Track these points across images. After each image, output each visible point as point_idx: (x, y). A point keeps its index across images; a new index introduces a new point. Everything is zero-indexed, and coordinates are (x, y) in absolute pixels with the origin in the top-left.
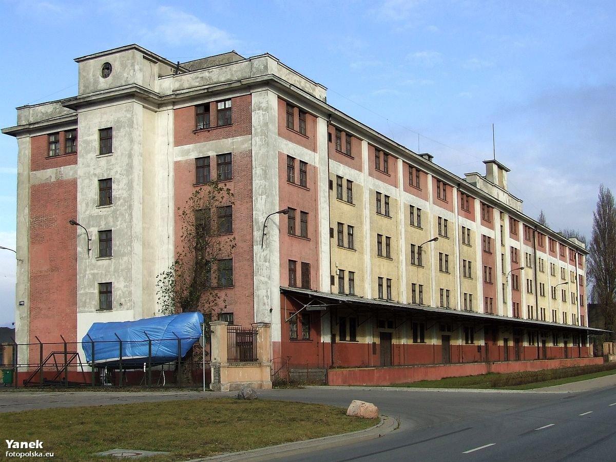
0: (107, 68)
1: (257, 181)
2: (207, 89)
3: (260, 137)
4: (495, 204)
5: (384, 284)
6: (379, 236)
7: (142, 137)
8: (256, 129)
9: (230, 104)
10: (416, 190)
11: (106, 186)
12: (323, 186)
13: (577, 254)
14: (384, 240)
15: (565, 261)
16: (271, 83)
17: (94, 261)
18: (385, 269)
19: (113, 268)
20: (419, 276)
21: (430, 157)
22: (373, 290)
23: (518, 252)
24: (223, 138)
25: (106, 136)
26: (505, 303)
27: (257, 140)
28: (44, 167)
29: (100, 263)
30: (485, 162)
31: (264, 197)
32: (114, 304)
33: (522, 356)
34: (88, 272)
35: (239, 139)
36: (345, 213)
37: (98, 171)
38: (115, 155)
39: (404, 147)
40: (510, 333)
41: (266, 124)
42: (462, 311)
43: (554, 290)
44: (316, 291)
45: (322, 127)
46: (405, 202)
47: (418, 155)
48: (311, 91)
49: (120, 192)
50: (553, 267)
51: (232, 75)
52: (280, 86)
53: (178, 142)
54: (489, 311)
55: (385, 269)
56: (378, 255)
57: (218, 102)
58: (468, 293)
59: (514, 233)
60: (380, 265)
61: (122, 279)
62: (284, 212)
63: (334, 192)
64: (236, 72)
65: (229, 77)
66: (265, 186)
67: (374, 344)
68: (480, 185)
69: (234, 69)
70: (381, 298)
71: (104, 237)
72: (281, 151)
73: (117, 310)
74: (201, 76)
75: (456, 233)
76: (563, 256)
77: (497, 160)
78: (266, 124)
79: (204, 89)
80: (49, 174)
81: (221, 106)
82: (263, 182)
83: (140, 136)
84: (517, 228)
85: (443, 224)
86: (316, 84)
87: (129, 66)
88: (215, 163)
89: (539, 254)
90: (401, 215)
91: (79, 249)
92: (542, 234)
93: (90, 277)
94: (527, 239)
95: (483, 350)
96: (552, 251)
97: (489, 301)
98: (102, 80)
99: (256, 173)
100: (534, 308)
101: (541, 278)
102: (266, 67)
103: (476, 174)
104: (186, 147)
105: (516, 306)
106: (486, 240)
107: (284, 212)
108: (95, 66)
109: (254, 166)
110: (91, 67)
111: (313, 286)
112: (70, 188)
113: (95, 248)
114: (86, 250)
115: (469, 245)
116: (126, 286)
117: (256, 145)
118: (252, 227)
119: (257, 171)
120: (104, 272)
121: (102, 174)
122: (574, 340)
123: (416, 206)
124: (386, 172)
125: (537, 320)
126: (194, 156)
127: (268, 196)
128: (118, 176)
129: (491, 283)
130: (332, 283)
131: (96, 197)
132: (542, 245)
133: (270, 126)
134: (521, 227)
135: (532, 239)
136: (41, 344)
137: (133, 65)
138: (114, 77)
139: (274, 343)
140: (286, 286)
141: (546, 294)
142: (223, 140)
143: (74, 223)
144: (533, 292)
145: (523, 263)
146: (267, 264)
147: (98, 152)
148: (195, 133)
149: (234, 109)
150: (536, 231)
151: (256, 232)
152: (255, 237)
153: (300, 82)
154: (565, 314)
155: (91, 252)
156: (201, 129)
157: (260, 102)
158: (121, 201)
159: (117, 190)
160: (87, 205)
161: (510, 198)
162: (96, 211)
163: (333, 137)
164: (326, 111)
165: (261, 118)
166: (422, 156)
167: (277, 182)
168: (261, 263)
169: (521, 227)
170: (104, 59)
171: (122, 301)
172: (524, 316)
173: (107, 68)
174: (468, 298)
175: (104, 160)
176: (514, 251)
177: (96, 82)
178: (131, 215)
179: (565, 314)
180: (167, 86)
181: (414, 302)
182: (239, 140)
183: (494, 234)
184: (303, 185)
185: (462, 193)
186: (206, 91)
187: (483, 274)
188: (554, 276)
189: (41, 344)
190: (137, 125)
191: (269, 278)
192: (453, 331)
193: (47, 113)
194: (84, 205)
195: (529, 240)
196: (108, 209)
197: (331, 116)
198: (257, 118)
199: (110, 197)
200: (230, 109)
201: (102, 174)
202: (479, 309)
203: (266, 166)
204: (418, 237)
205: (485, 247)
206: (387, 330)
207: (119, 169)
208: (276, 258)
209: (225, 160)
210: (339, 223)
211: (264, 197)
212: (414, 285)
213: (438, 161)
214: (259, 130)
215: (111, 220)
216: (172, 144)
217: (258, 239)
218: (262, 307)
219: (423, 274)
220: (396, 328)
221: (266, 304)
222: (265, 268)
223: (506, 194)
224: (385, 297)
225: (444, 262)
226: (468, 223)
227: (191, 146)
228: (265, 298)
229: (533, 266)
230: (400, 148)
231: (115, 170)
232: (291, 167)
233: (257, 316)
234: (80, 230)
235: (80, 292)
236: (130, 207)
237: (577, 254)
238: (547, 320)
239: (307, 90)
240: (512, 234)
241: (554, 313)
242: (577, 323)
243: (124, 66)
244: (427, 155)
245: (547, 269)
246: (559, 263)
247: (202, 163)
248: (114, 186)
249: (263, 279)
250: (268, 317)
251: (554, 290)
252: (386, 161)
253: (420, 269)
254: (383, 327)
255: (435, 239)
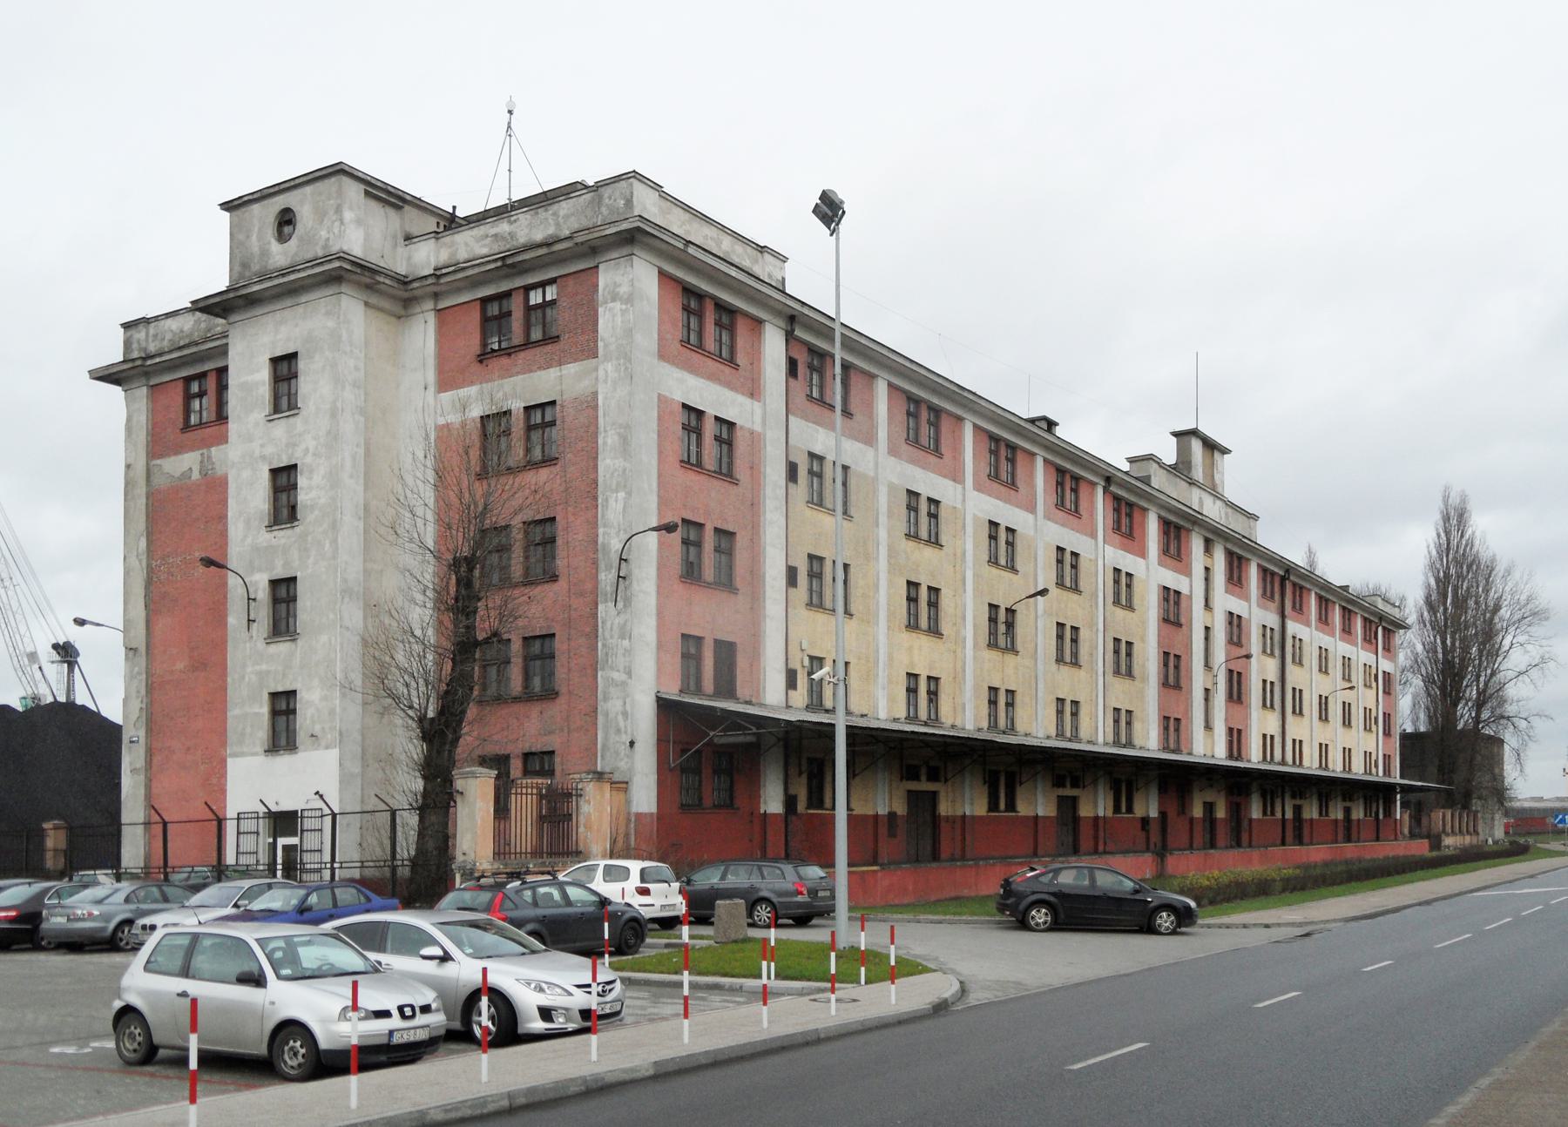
0: (286, 220)
1: (608, 461)
2: (503, 258)
3: (614, 362)
4: (1195, 521)
5: (999, 699)
6: (1060, 626)
7: (363, 371)
8: (606, 346)
9: (555, 292)
10: (727, 370)
11: (284, 479)
12: (775, 473)
13: (1380, 629)
14: (924, 594)
15: (1332, 634)
16: (635, 237)
17: (261, 645)
18: (923, 655)
19: (298, 659)
20: (1005, 671)
21: (1051, 424)
22: (891, 700)
23: (1244, 623)
24: (540, 368)
25: (284, 368)
26: (1208, 727)
27: (607, 369)
28: (178, 449)
29: (273, 649)
30: (1176, 434)
31: (621, 495)
32: (301, 737)
33: (1245, 837)
34: (249, 669)
35: (571, 369)
36: (926, 564)
37: (269, 450)
38: (303, 413)
39: (974, 394)
40: (1219, 791)
41: (629, 333)
42: (1106, 744)
43: (1324, 703)
44: (748, 703)
45: (774, 345)
46: (977, 513)
47: (1025, 420)
48: (746, 263)
49: (313, 494)
50: (1323, 655)
51: (558, 225)
52: (664, 246)
53: (447, 380)
54: (1172, 746)
55: (923, 655)
56: (989, 645)
57: (528, 289)
58: (1124, 707)
59: (1235, 578)
60: (910, 649)
61: (316, 682)
62: (669, 528)
63: (801, 489)
64: (567, 217)
65: (551, 230)
66: (624, 470)
67: (892, 816)
68: (1159, 480)
69: (562, 213)
70: (912, 718)
71: (282, 592)
72: (667, 394)
73: (305, 751)
74: (493, 231)
75: (1096, 579)
76: (1347, 630)
77: (1205, 429)
78: (629, 333)
79: (496, 260)
80: (184, 464)
81: (535, 298)
82: (620, 463)
83: (357, 369)
84: (1243, 574)
85: (1067, 564)
86: (762, 249)
87: (331, 212)
88: (521, 424)
89: (1293, 627)
90: (968, 544)
91: (231, 620)
92: (1350, 611)
93: (254, 678)
94: (1266, 594)
95: (1154, 829)
96: (1324, 620)
97: (1172, 726)
98: (275, 246)
99: (605, 443)
100: (1278, 740)
101: (1295, 676)
102: (629, 203)
103: (1150, 458)
104: (463, 392)
105: (1236, 737)
106: (1171, 599)
107: (669, 528)
108: (266, 214)
109: (601, 429)
110: (256, 221)
111: (741, 691)
112: (216, 487)
113: (263, 613)
114: (245, 622)
115: (1130, 607)
116: (324, 698)
117: (605, 382)
118: (595, 563)
119: (608, 439)
120: (280, 668)
121: (278, 455)
122: (1366, 803)
123: (1003, 523)
124: (1012, 484)
125: (1283, 762)
126: (476, 412)
127: (629, 494)
128: (309, 459)
129: (1177, 687)
130: (791, 682)
131: (267, 506)
132: (1299, 608)
133: (638, 338)
134: (1253, 573)
135: (1277, 597)
136: (165, 824)
137: (338, 210)
138: (301, 239)
139: (639, 816)
140: (672, 692)
141: (1353, 723)
142: (539, 373)
143: (214, 563)
144: (1276, 707)
145: (1254, 643)
146: (626, 643)
147: (267, 408)
148: (481, 362)
149: (563, 303)
150: (1288, 579)
151: (603, 574)
152: (602, 586)
153: (719, 243)
154: (1347, 753)
155: (254, 626)
156: (493, 351)
157: (615, 283)
158: (316, 512)
159: (308, 491)
160: (248, 522)
161: (1230, 510)
162: (265, 538)
163: (802, 369)
164: (780, 307)
165: (619, 319)
166: (1032, 421)
167: (655, 462)
168: (614, 641)
169: (1253, 573)
170: (280, 202)
171: (317, 729)
172: (1254, 757)
173: (286, 220)
174: (1123, 719)
175: (280, 429)
176: (1235, 621)
177: (265, 253)
178: (334, 541)
179: (1347, 753)
180: (425, 257)
181: (993, 725)
182: (573, 371)
183: (1190, 585)
184: (726, 473)
185: (1117, 498)
186: (499, 264)
187: (1159, 667)
188: (1326, 672)
189: (165, 824)
190: (351, 346)
191: (629, 673)
192: (1084, 787)
193: (182, 331)
194: (241, 525)
195: (1370, 642)
196: (289, 532)
197: (795, 319)
198: (609, 320)
199: (293, 509)
200: (553, 302)
201: (278, 455)
202: (1148, 742)
203: (627, 427)
204: (1006, 589)
205: (1231, 634)
206: (925, 786)
207: (311, 444)
208: (646, 629)
209: (541, 416)
210: (1115, 639)
211: (621, 495)
212: (993, 690)
213: (1074, 432)
214: (613, 347)
215: (295, 554)
216: (432, 389)
217: (608, 588)
218: (613, 738)
219: (1016, 668)
220: (946, 781)
221: (623, 729)
222: (621, 652)
223: (1219, 503)
224: (923, 715)
225: (1068, 642)
226: (1128, 562)
227: (472, 390)
228: (620, 717)
229: (1277, 652)
230: (966, 394)
231: (303, 446)
232: (912, 508)
233: (602, 756)
234: (233, 580)
235: (233, 712)
236: (334, 526)
237: (1380, 629)
238: (1306, 763)
239: (736, 260)
240: (1230, 586)
241: (1324, 749)
242: (1374, 770)
243: (321, 215)
244: (1044, 419)
245: (1311, 658)
246: (1340, 648)
247: (493, 424)
248: (302, 481)
249: (616, 675)
250: (626, 760)
251: (1324, 703)
252: (1326, 605)
253: (1010, 658)
254: (916, 778)
255: (1043, 592)
